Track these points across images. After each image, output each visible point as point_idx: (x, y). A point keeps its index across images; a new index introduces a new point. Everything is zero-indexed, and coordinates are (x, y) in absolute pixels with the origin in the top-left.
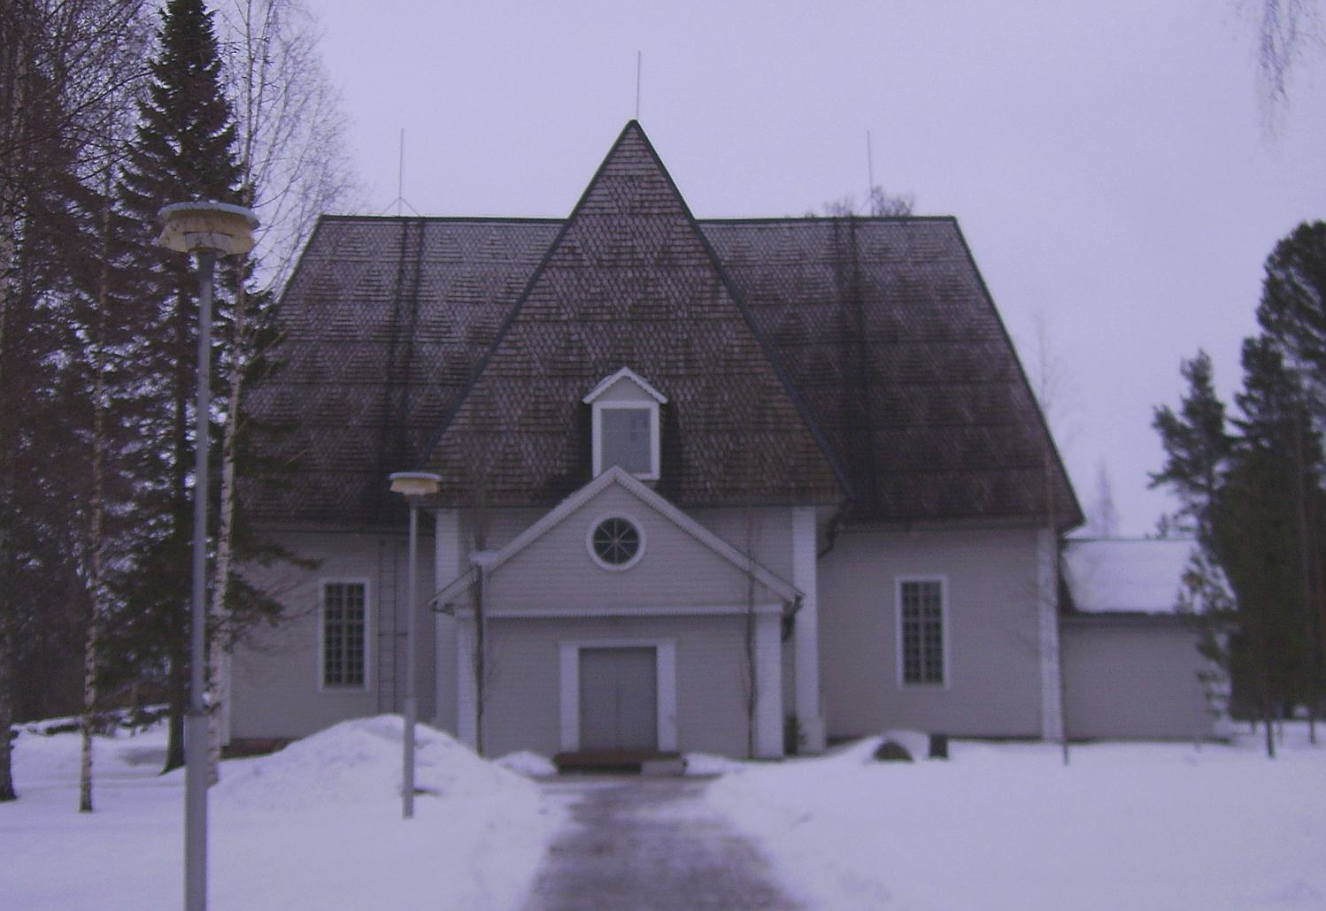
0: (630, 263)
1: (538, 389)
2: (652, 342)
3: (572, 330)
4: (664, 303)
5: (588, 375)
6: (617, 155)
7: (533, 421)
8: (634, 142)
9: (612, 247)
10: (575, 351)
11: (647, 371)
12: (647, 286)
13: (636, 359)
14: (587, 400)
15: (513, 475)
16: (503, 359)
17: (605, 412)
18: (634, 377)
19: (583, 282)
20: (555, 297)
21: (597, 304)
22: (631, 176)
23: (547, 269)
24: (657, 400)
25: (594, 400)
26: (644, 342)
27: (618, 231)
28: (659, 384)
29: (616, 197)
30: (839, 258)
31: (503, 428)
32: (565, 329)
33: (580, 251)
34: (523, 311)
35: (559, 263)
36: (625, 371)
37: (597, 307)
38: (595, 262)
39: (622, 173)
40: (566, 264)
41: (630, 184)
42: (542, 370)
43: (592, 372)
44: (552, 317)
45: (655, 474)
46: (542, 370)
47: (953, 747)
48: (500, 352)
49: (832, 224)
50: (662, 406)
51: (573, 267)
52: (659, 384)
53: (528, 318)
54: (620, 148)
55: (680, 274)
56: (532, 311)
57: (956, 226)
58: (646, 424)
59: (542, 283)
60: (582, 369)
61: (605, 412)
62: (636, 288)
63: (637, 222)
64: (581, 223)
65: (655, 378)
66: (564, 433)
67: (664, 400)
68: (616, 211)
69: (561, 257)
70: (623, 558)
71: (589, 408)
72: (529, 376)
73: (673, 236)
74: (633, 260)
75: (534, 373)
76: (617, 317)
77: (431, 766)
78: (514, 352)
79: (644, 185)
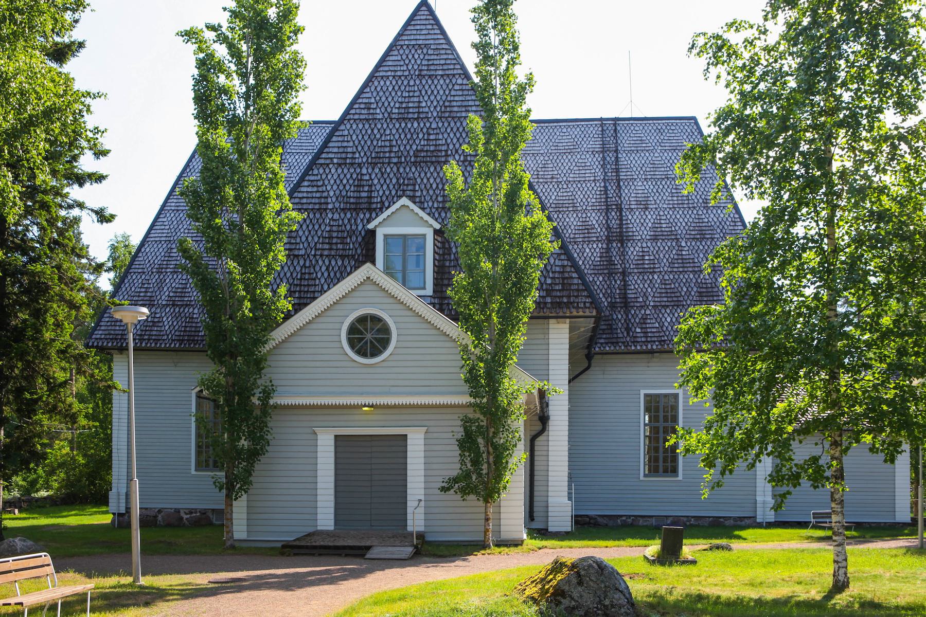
0: (416, 116)
1: (332, 219)
2: (432, 180)
3: (364, 171)
4: (444, 148)
5: (373, 208)
6: (409, 28)
7: (327, 246)
8: (424, 17)
9: (401, 103)
10: (366, 189)
11: (426, 205)
12: (429, 134)
13: (418, 194)
14: (371, 226)
15: (308, 291)
16: (305, 195)
17: (386, 237)
18: (412, 206)
19: (376, 131)
20: (351, 144)
21: (387, 149)
22: (419, 45)
23: (345, 122)
24: (431, 226)
25: (376, 227)
26: (425, 181)
27: (407, 90)
28: (437, 215)
29: (407, 62)
30: (603, 148)
31: (302, 252)
32: (358, 170)
33: (374, 106)
34: (323, 156)
35: (356, 117)
36: (404, 201)
37: (386, 152)
38: (386, 115)
39: (413, 42)
40: (362, 117)
41: (419, 52)
42: (337, 205)
43: (379, 206)
44: (348, 161)
45: (429, 291)
46: (337, 205)
47: (688, 549)
48: (303, 189)
49: (600, 123)
50: (436, 232)
51: (367, 120)
52: (437, 215)
53: (328, 161)
54: (413, 23)
55: (458, 124)
56: (331, 156)
57: (696, 123)
58: (423, 247)
59: (340, 133)
60: (371, 203)
61: (386, 237)
62: (421, 136)
63: (424, 82)
64: (376, 83)
65: (433, 210)
66: (353, 256)
67: (438, 226)
68: (406, 73)
69: (358, 111)
70: (375, 353)
71: (373, 233)
72: (325, 210)
73: (453, 93)
74: (419, 113)
75: (330, 206)
76: (403, 160)
77: (516, 545)
78: (315, 189)
79: (430, 52)
